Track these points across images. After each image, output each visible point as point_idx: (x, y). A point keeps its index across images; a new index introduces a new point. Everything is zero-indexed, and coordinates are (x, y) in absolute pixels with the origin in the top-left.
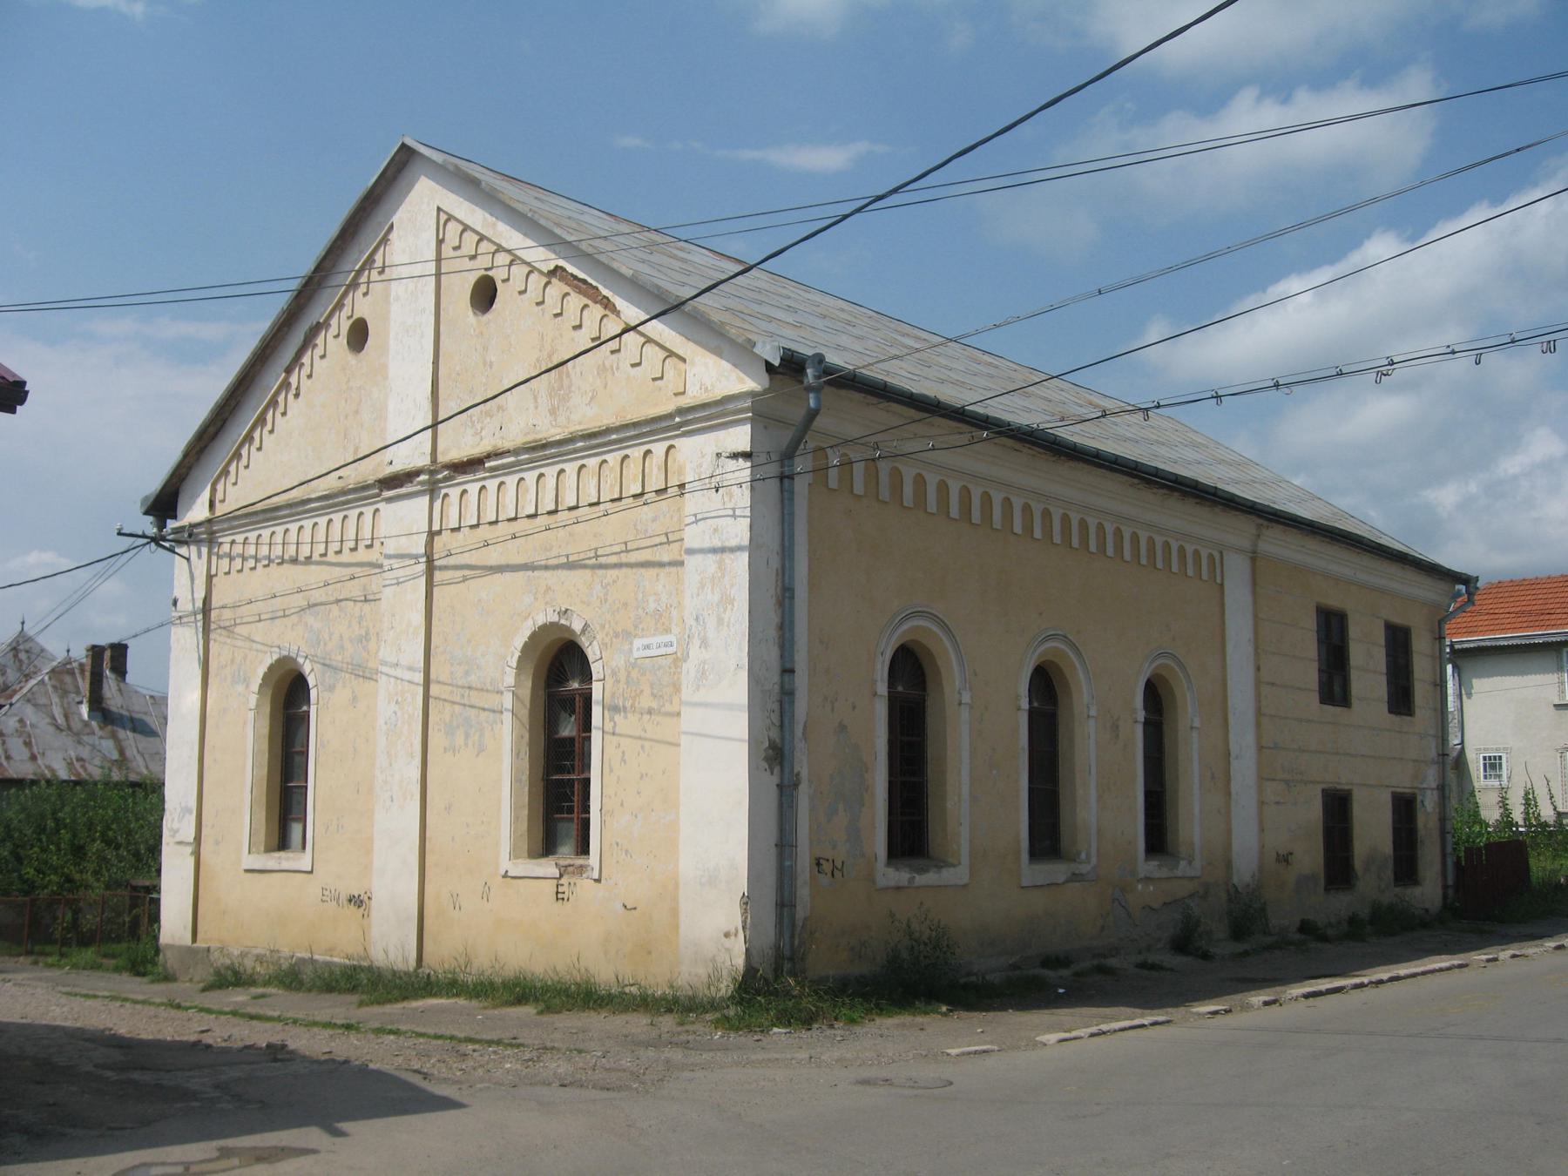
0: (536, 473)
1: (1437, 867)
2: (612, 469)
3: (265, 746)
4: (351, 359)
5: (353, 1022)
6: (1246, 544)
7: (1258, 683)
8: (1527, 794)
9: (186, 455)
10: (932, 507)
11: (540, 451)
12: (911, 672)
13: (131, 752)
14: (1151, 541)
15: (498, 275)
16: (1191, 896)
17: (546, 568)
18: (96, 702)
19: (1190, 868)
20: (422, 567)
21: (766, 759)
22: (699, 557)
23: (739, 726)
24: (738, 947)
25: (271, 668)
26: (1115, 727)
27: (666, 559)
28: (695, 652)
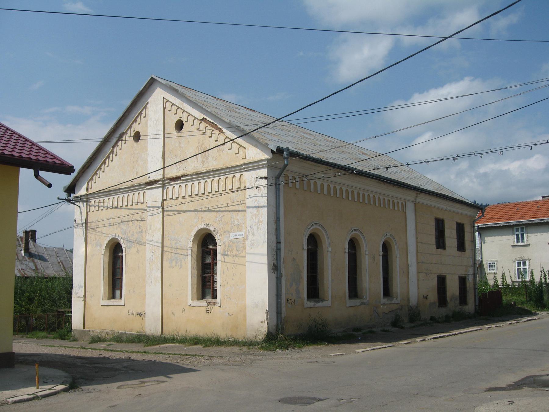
1: (473, 299)
2: (222, 181)
6: (413, 199)
7: (417, 242)
8: (503, 275)
10: (319, 191)
11: (199, 175)
12: (313, 241)
13: (39, 267)
15: (184, 119)
16: (397, 309)
17: (202, 211)
18: (27, 250)
19: (396, 301)
20: (161, 210)
21: (273, 269)
23: (265, 260)
24: (265, 325)
25: (109, 241)
26: (374, 257)
27: (240, 209)
28: (250, 237)
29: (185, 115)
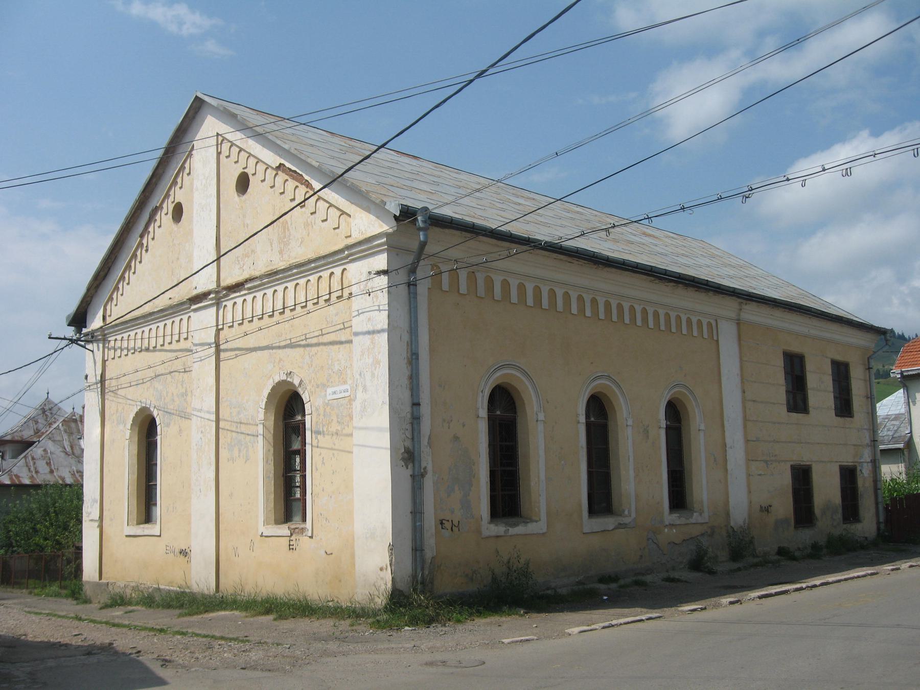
0: (272, 290)
1: (873, 510)
3: (135, 461)
4: (174, 227)
5: (165, 627)
6: (733, 315)
7: (744, 401)
9: (88, 290)
10: (514, 299)
11: (274, 276)
14: (667, 315)
15: (250, 171)
16: (702, 535)
17: (279, 347)
19: (700, 517)
20: (213, 350)
21: (403, 459)
22: (361, 337)
23: (385, 440)
24: (388, 576)
25: (137, 414)
26: (646, 432)
27: (343, 339)
28: (360, 395)
29: (252, 161)
